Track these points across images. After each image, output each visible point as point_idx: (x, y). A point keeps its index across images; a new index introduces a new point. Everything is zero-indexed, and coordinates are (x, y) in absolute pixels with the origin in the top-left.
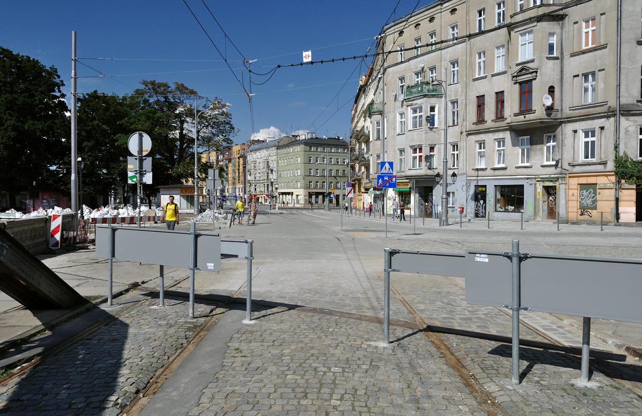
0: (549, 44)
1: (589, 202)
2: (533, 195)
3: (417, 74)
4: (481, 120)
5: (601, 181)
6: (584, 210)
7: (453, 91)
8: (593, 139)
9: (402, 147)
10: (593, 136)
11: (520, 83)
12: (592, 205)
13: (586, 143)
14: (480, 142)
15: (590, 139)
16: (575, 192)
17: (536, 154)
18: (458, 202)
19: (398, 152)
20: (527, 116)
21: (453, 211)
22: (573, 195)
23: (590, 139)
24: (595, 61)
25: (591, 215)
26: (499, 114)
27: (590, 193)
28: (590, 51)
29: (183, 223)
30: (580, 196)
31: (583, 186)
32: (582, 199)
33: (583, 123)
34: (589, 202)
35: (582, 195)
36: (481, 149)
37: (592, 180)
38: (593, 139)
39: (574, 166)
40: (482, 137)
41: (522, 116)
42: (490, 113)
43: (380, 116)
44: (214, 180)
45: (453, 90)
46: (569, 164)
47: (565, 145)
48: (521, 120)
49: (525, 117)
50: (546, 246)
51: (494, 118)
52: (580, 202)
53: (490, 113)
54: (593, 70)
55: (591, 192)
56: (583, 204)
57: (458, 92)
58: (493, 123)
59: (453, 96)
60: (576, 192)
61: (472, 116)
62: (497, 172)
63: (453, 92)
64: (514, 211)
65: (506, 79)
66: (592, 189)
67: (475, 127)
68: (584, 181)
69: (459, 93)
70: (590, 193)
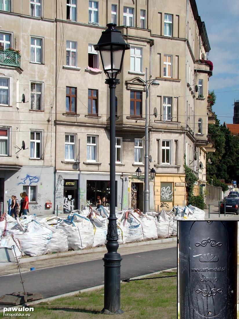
0: (89, 54)
4: (73, 111)
5: (177, 180)
6: (163, 203)
9: (158, 138)
10: (168, 145)
11: (132, 91)
12: (169, 199)
13: (163, 150)
15: (165, 148)
16: (158, 188)
17: (128, 154)
18: (42, 198)
20: (138, 121)
21: (35, 208)
22: (157, 191)
23: (165, 148)
24: (173, 89)
25: (168, 207)
27: (168, 189)
29: (24, 271)
31: (163, 184)
32: (163, 194)
34: (167, 196)
35: (163, 190)
37: (170, 180)
40: (73, 130)
45: (36, 70)
47: (151, 150)
49: (136, 122)
51: (87, 113)
52: (161, 196)
54: (171, 96)
55: (169, 188)
56: (163, 198)
57: (44, 75)
58: (64, 116)
61: (62, 106)
63: (37, 73)
65: (100, 79)
66: (169, 186)
68: (165, 179)
69: (45, 76)
70: (168, 189)
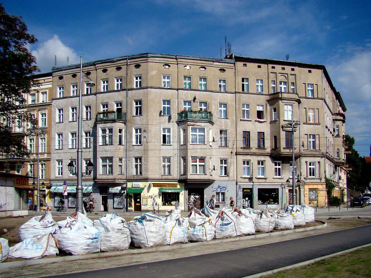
1: (313, 197)
2: (284, 195)
3: (185, 102)
5: (320, 187)
7: (220, 123)
8: (310, 167)
14: (87, 160)
19: (134, 159)
23: (312, 167)
24: (315, 130)
26: (40, 148)
27: (314, 193)
28: (313, 124)
30: (309, 194)
31: (311, 190)
32: (310, 196)
33: (310, 158)
34: (313, 197)
36: (59, 165)
37: (315, 187)
38: (310, 167)
39: (306, 179)
40: (248, 158)
41: (289, 150)
42: (254, 143)
43: (123, 124)
44: (177, 90)
45: (223, 122)
46: (304, 178)
48: (288, 152)
50: (311, 224)
52: (309, 197)
53: (254, 143)
59: (223, 126)
60: (308, 192)
62: (260, 181)
63: (223, 124)
64: (273, 204)
67: (242, 150)
68: (311, 187)
70: (314, 193)
